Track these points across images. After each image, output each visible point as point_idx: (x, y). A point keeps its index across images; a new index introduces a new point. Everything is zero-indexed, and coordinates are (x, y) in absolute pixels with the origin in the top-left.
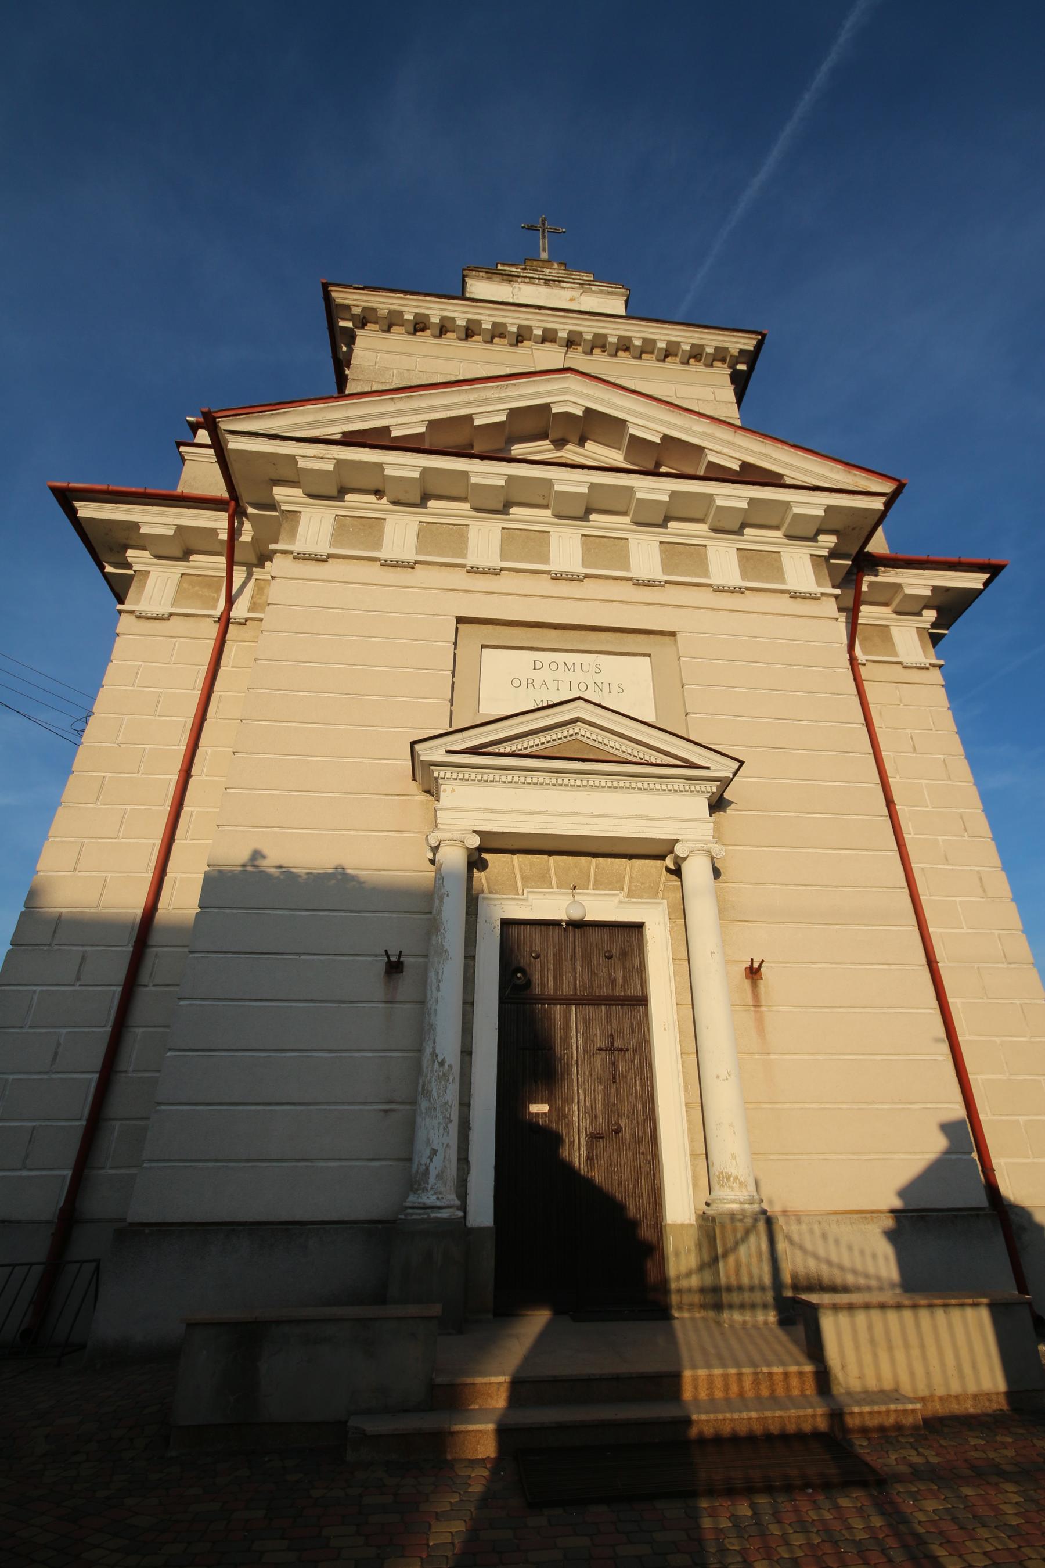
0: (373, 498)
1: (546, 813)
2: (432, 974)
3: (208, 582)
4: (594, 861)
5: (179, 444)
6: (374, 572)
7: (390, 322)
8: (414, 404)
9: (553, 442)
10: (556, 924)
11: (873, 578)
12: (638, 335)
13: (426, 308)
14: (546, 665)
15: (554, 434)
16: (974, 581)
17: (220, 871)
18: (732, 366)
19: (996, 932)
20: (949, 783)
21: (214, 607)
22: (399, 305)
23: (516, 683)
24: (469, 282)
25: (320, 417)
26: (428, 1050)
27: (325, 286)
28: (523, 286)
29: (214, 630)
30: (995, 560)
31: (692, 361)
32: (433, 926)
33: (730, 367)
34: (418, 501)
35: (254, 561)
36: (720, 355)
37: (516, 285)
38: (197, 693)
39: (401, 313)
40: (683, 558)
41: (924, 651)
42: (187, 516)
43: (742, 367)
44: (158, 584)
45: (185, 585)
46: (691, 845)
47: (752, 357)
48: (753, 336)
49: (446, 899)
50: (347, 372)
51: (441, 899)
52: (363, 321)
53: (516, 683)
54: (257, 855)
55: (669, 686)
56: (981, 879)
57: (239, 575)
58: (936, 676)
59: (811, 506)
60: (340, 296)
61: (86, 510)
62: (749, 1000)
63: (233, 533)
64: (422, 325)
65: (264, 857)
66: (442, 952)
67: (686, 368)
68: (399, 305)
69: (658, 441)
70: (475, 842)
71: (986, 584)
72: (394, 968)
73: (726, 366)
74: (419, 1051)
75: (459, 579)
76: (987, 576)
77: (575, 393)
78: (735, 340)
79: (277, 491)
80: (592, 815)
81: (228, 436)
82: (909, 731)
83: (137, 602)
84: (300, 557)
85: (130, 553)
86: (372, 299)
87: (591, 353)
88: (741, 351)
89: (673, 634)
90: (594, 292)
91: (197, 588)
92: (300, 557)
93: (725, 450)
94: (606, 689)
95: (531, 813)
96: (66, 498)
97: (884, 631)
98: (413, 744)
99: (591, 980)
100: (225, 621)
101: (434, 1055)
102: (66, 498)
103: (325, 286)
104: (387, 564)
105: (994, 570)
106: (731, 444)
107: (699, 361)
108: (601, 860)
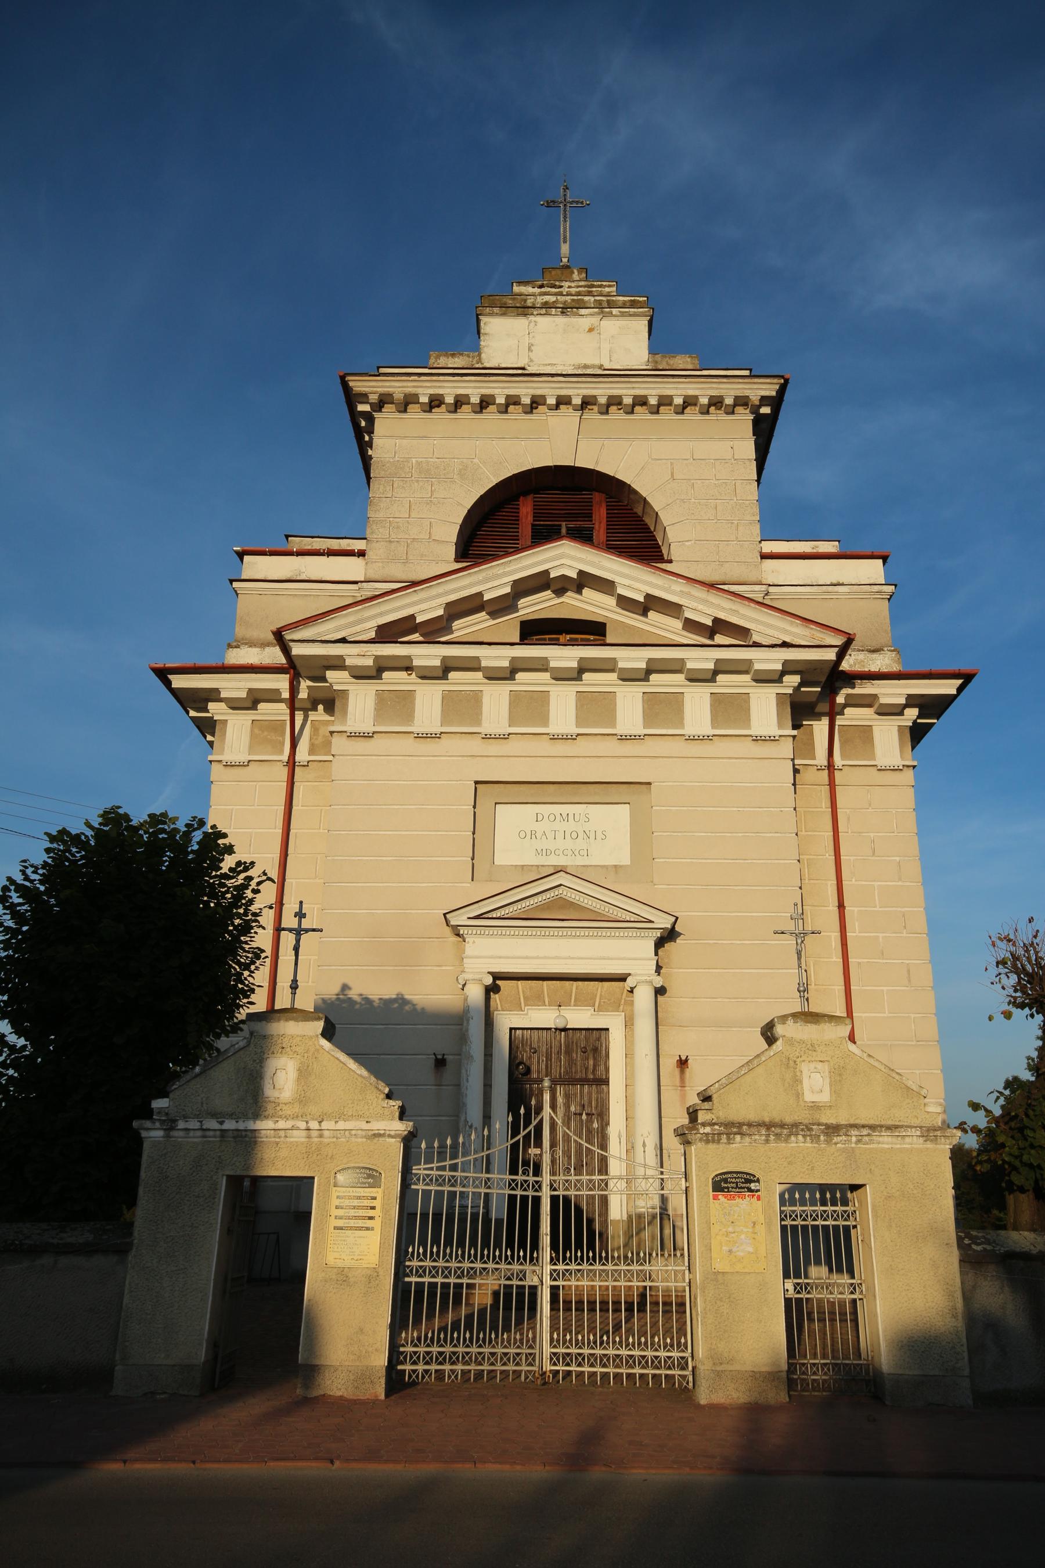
0: (403, 674)
1: (537, 958)
2: (463, 1071)
3: (275, 726)
4: (575, 984)
5: (231, 581)
6: (408, 744)
7: (407, 403)
8: (434, 592)
9: (554, 592)
10: (550, 1029)
11: (850, 691)
12: (654, 392)
13: (440, 387)
14: (546, 817)
15: (553, 587)
16: (948, 687)
17: (323, 999)
18: (755, 410)
19: (913, 1016)
20: (900, 883)
21: (282, 752)
22: (414, 387)
23: (522, 835)
24: (484, 319)
25: (359, 616)
26: (463, 1119)
27: (343, 378)
28: (539, 319)
29: (284, 772)
30: (965, 667)
31: (712, 409)
32: (463, 1038)
33: (752, 413)
34: (441, 675)
35: (309, 706)
36: (741, 401)
37: (532, 318)
38: (279, 831)
39: (416, 396)
40: (663, 710)
41: (901, 751)
42: (255, 680)
43: (766, 410)
44: (237, 731)
45: (256, 731)
46: (639, 978)
47: (776, 402)
48: (776, 381)
49: (471, 1021)
50: (370, 452)
51: (468, 1021)
52: (379, 406)
53: (522, 835)
54: (345, 987)
55: (641, 835)
56: (909, 971)
57: (299, 717)
58: (909, 776)
59: (770, 661)
60: (358, 385)
61: (179, 682)
62: (678, 1083)
63: (294, 690)
64: (437, 403)
65: (350, 988)
66: (470, 1057)
67: (707, 417)
68: (414, 387)
69: (642, 600)
70: (489, 980)
71: (960, 689)
72: (440, 1063)
73: (748, 411)
74: (458, 1116)
75: (475, 745)
76: (960, 681)
77: (572, 558)
78: (756, 386)
79: (329, 674)
80: (570, 958)
81: (291, 644)
82: (872, 835)
83: (222, 752)
84: (353, 736)
85: (211, 706)
86: (387, 384)
87: (607, 413)
88: (763, 398)
89: (649, 784)
90: (615, 316)
91: (266, 733)
92: (353, 736)
93: (700, 607)
94: (592, 836)
95: (527, 958)
96: (163, 674)
97: (866, 733)
98: (445, 915)
99: (571, 1068)
100: (292, 764)
101: (466, 1121)
102: (163, 674)
103: (343, 378)
104: (419, 737)
105: (967, 678)
106: (705, 602)
107: (720, 409)
108: (580, 983)
